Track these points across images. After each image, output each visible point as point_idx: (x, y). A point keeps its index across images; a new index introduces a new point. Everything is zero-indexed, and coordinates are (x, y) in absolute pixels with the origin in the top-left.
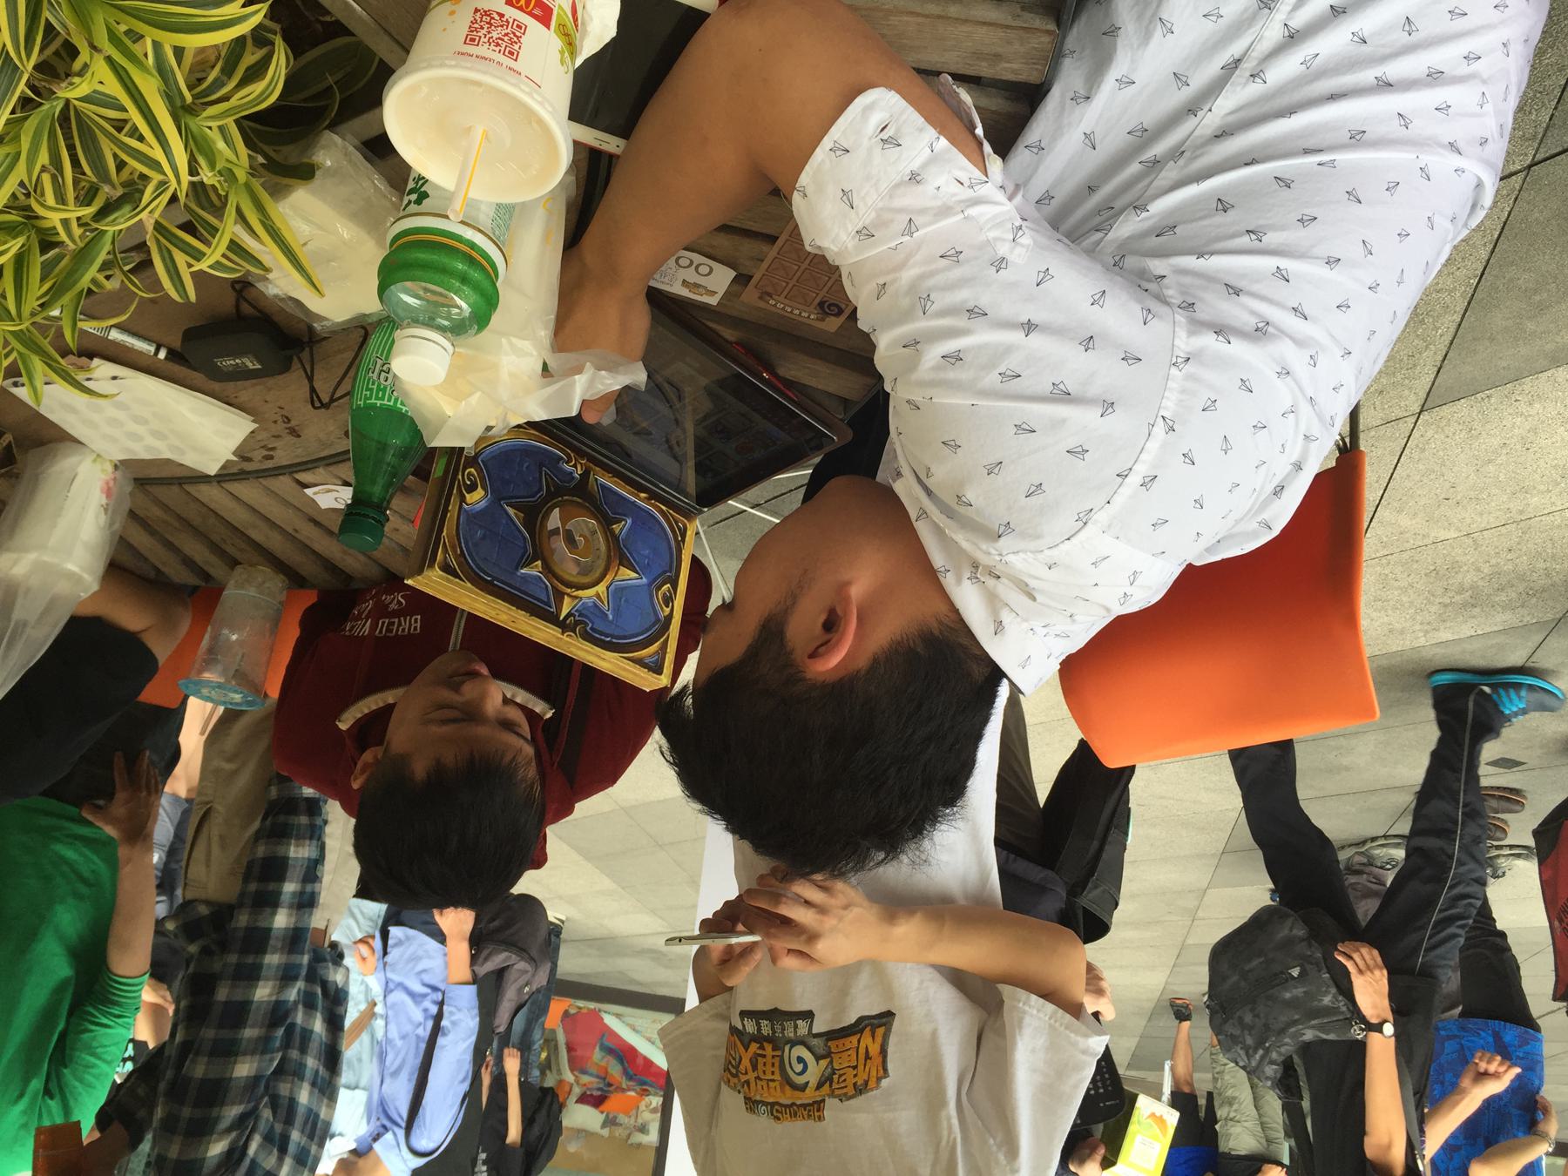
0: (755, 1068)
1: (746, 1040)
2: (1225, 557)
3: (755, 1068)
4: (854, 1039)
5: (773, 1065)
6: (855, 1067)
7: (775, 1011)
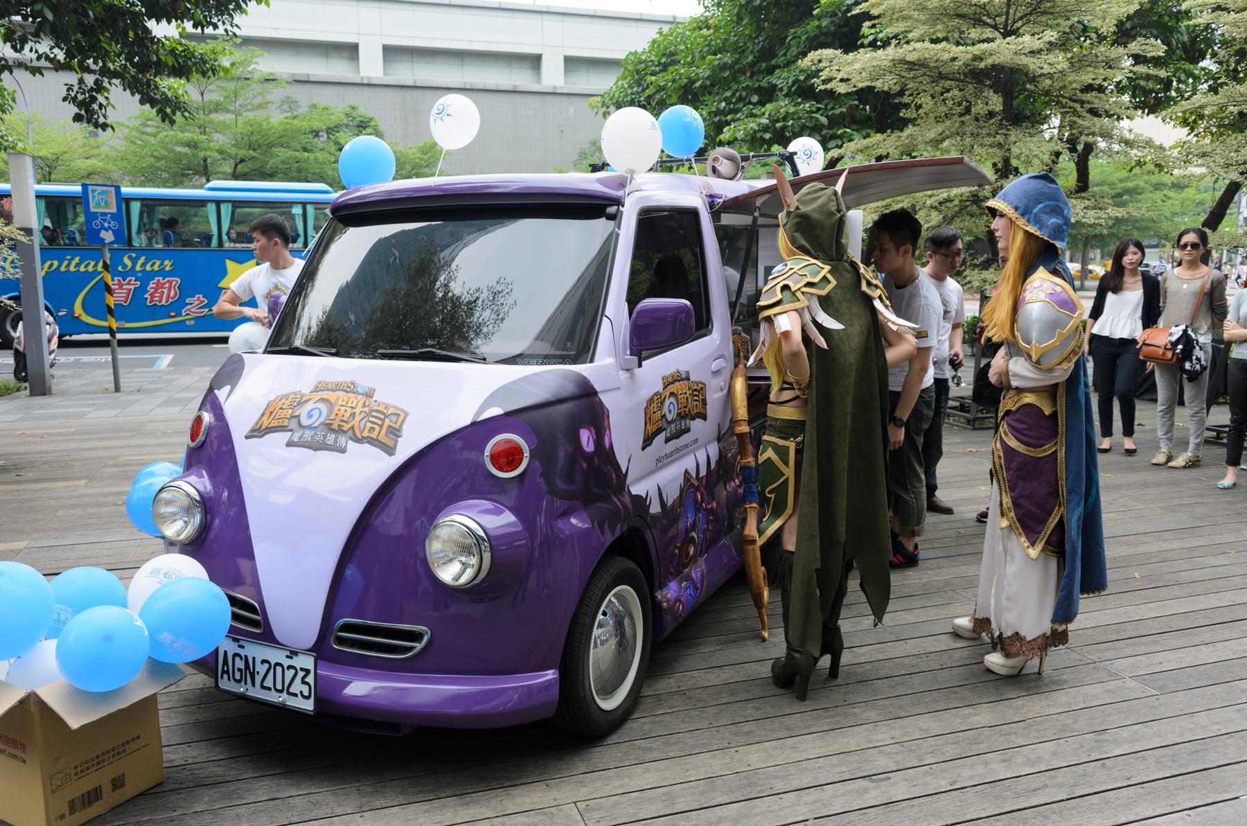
0: (353, 415)
1: (350, 433)
2: (122, 707)
3: (353, 415)
5: (337, 415)
6: (281, 408)
7: (316, 449)
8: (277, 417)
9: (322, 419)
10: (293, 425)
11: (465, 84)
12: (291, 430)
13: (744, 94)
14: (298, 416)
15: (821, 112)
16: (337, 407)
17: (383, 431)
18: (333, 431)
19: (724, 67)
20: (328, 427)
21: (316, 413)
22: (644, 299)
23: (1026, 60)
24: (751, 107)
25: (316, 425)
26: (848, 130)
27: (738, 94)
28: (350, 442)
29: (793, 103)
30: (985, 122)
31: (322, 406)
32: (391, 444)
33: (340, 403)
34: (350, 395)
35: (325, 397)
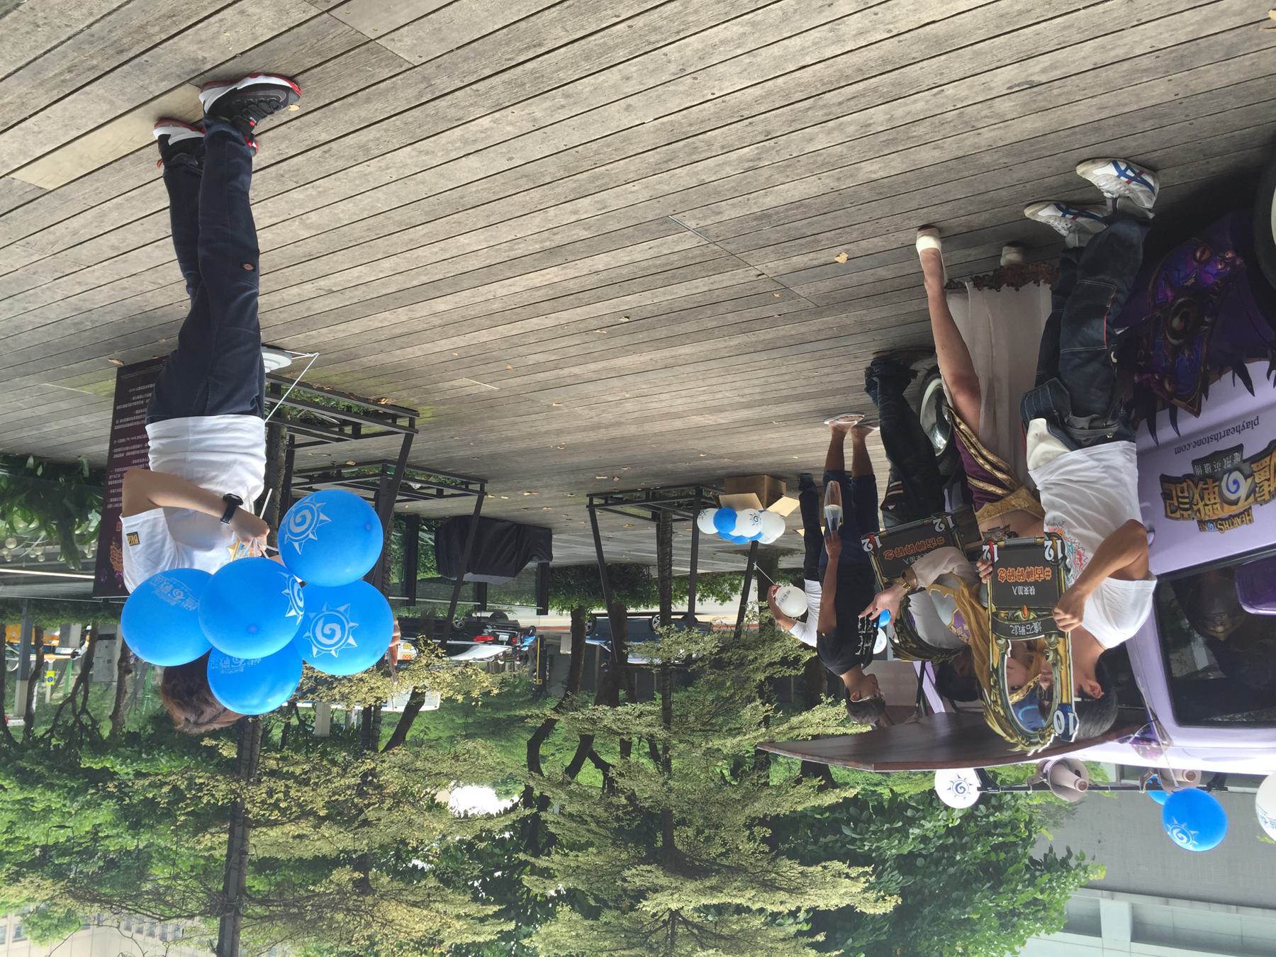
0: (1202, 499)
3: (1202, 499)
4: (1267, 459)
6: (1268, 480)
8: (1267, 469)
9: (1223, 484)
10: (1246, 467)
11: (1237, 911)
12: (1245, 461)
13: (933, 868)
14: (1246, 478)
15: (848, 839)
16: (1218, 500)
17: (1174, 492)
18: (1210, 476)
19: (957, 903)
20: (1216, 478)
21: (1233, 488)
22: (916, 634)
23: (663, 881)
24: (924, 852)
25: (1226, 476)
26: (819, 816)
27: (941, 869)
28: (1192, 472)
29: (881, 851)
30: (298, 791)
31: (1233, 497)
32: (1166, 485)
33: (1218, 505)
34: (1216, 517)
35: (1234, 507)
